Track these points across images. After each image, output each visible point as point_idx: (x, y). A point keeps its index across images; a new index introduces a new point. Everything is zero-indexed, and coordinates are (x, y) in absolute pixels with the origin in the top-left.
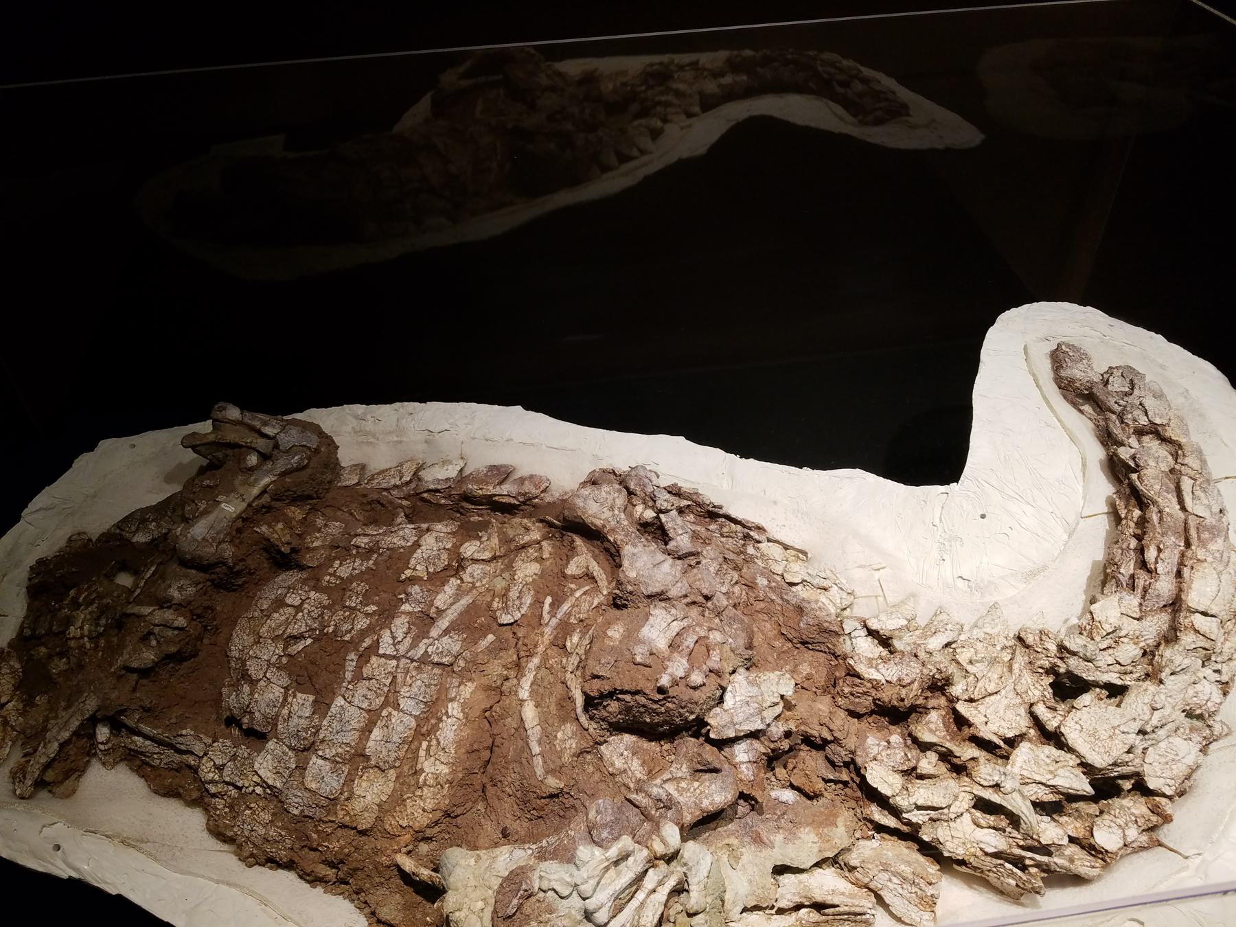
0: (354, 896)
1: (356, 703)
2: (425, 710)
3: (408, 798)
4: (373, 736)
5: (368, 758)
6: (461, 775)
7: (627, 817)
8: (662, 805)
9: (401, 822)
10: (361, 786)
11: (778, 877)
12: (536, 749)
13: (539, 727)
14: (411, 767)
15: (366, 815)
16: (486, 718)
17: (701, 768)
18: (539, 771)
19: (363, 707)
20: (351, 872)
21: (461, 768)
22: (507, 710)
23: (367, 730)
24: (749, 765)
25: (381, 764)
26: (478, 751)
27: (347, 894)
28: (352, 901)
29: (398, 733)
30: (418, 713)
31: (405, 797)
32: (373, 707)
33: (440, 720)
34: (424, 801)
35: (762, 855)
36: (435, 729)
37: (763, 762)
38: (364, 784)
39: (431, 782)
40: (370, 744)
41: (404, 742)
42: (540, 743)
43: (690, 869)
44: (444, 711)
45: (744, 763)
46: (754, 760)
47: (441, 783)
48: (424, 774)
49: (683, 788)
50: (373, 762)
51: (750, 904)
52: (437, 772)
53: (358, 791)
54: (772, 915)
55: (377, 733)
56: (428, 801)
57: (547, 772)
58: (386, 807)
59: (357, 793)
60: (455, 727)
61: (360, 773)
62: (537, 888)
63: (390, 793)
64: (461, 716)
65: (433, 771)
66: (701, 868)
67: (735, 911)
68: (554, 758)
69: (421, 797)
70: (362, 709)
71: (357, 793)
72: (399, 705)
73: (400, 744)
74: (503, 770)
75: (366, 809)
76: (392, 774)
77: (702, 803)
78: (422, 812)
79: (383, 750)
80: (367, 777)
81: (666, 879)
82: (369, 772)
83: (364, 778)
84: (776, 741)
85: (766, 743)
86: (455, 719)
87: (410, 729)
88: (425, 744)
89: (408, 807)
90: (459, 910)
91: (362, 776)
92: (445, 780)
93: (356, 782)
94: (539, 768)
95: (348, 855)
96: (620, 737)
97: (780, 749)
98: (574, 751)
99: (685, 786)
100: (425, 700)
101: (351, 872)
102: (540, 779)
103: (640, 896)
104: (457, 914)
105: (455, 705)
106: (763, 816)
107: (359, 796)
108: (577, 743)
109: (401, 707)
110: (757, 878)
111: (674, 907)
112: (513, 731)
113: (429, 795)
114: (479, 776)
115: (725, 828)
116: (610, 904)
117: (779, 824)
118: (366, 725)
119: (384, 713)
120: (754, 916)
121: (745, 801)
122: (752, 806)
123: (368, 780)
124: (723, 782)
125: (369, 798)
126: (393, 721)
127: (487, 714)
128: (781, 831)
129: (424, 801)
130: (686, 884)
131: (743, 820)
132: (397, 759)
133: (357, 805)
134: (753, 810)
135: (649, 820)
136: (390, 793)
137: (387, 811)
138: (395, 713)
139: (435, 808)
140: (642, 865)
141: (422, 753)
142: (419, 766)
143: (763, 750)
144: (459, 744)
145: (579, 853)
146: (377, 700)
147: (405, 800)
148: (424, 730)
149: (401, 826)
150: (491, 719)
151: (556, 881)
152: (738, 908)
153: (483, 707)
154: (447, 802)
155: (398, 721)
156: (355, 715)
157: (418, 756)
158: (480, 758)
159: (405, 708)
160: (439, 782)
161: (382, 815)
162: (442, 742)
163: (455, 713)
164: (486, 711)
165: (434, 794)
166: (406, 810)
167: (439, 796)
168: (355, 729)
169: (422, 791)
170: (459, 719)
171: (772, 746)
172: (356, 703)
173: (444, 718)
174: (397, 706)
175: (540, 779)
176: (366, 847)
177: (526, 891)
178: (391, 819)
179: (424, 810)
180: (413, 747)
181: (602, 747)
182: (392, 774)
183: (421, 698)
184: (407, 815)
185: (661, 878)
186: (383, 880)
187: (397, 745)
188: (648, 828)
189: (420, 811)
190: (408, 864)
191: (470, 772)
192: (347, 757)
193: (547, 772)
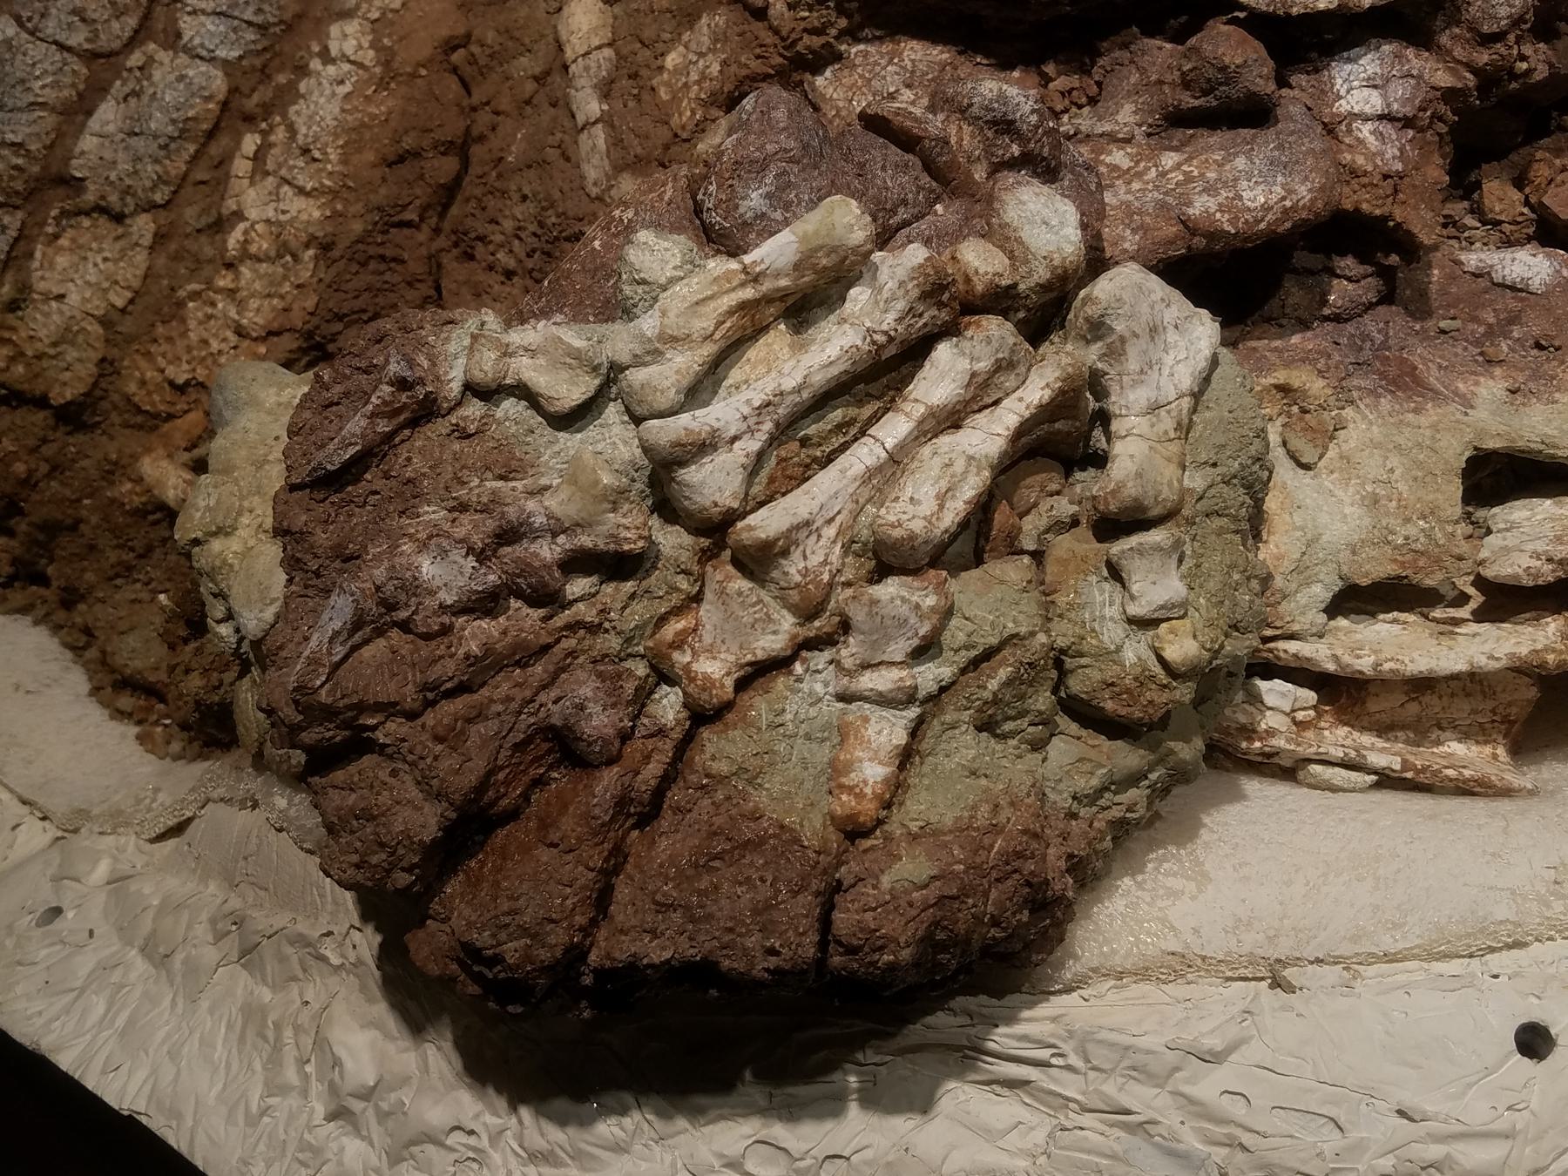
0: (60, 616)
1: (49, 31)
2: (259, 47)
3: (195, 296)
4: (94, 123)
5: (75, 185)
6: (357, 227)
7: (862, 166)
8: (1015, 150)
9: (171, 371)
10: (52, 265)
11: (1481, 514)
12: (589, 105)
13: (608, 52)
14: (205, 211)
15: (72, 354)
16: (455, 70)
17: (1189, 101)
18: (594, 170)
19: (72, 42)
20: (41, 537)
21: (358, 208)
22: (517, 34)
23: (79, 109)
24: (1387, 129)
25: (113, 198)
26: (416, 154)
27: (41, 611)
28: (56, 629)
29: (164, 110)
30: (235, 54)
31: (182, 293)
32: (105, 43)
33: (302, 70)
34: (241, 305)
35: (1423, 420)
36: (289, 94)
37: (1443, 128)
38: (62, 261)
39: (262, 245)
40: (88, 143)
41: (183, 135)
42: (606, 90)
43: (1115, 352)
44: (316, 48)
45: (1366, 119)
46: (1408, 111)
47: (293, 244)
48: (242, 226)
49: (1114, 168)
50: (90, 197)
51: (1375, 568)
52: (282, 218)
53: (44, 281)
54: (1456, 622)
55: (107, 114)
56: (254, 304)
57: (619, 168)
58: (127, 325)
59: (42, 286)
60: (347, 88)
61: (50, 230)
62: (455, 387)
63: (136, 284)
64: (369, 56)
65: (271, 214)
66: (1169, 360)
67: (1302, 598)
68: (646, 124)
69: (231, 293)
70: (69, 49)
71: (42, 286)
72: (179, 35)
73: (172, 138)
74: (491, 202)
75: (66, 336)
76: (143, 226)
77: (1189, 204)
78: (233, 339)
79: (121, 155)
80: (73, 240)
81: (1010, 381)
82: (78, 227)
83: (64, 242)
84: (1498, 37)
85: (1458, 52)
86: (346, 67)
87: (208, 99)
88: (250, 142)
89: (192, 324)
90: (222, 531)
91: (56, 237)
92: (304, 237)
93: (38, 255)
94: (595, 161)
95: (28, 482)
96: (887, 47)
97: (1513, 76)
98: (716, 85)
99: (1126, 163)
100: (259, 19)
101: (41, 537)
102: (594, 191)
103: (894, 429)
104: (216, 545)
105: (352, 27)
106: (1430, 324)
107: (47, 297)
108: (724, 63)
109: (186, 39)
110: (1402, 486)
111: (1044, 506)
112: (530, 86)
113: (257, 286)
114: (422, 236)
115: (1277, 343)
116: (753, 445)
117: (1490, 351)
118: (80, 95)
119: (136, 59)
120: (1378, 627)
121: (1363, 259)
122: (1386, 274)
123: (76, 247)
124: (1280, 147)
125: (74, 298)
126: (157, 75)
127: (458, 57)
128: (1498, 371)
129: (241, 305)
130: (1098, 433)
131: (1350, 328)
132: (161, 180)
133: (42, 324)
134: (1388, 298)
135: (954, 194)
136: (136, 284)
137: (131, 340)
138: (164, 56)
139: (275, 325)
140: (901, 305)
141: (241, 166)
142: (231, 205)
143: (1444, 79)
144: (354, 137)
145: (633, 254)
146: (116, 25)
147: (181, 304)
148: (251, 103)
149: (172, 383)
150: (468, 71)
151: (531, 352)
152: (1317, 589)
153: (445, 32)
154: (310, 303)
155: (172, 77)
156: (46, 65)
157: (228, 176)
158: (422, 177)
159: (197, 41)
160: (285, 244)
161: (115, 352)
162: (303, 130)
163: (349, 47)
164: (455, 48)
165: (271, 284)
166: (184, 334)
167: (287, 287)
168: (43, 105)
169: (237, 278)
170: (360, 65)
171: (1483, 57)
172: (49, 31)
173: (315, 64)
174: (173, 40)
175: (594, 191)
176: (85, 463)
177: (402, 384)
178: (143, 363)
179: (240, 332)
180: (214, 150)
181: (820, 81)
182: (143, 226)
183: (248, 15)
184: (189, 349)
185: (983, 365)
186: (129, 557)
187: (161, 141)
188: (953, 219)
189: (229, 334)
190: (172, 481)
191: (390, 221)
192: (19, 185)
193: (619, 168)
